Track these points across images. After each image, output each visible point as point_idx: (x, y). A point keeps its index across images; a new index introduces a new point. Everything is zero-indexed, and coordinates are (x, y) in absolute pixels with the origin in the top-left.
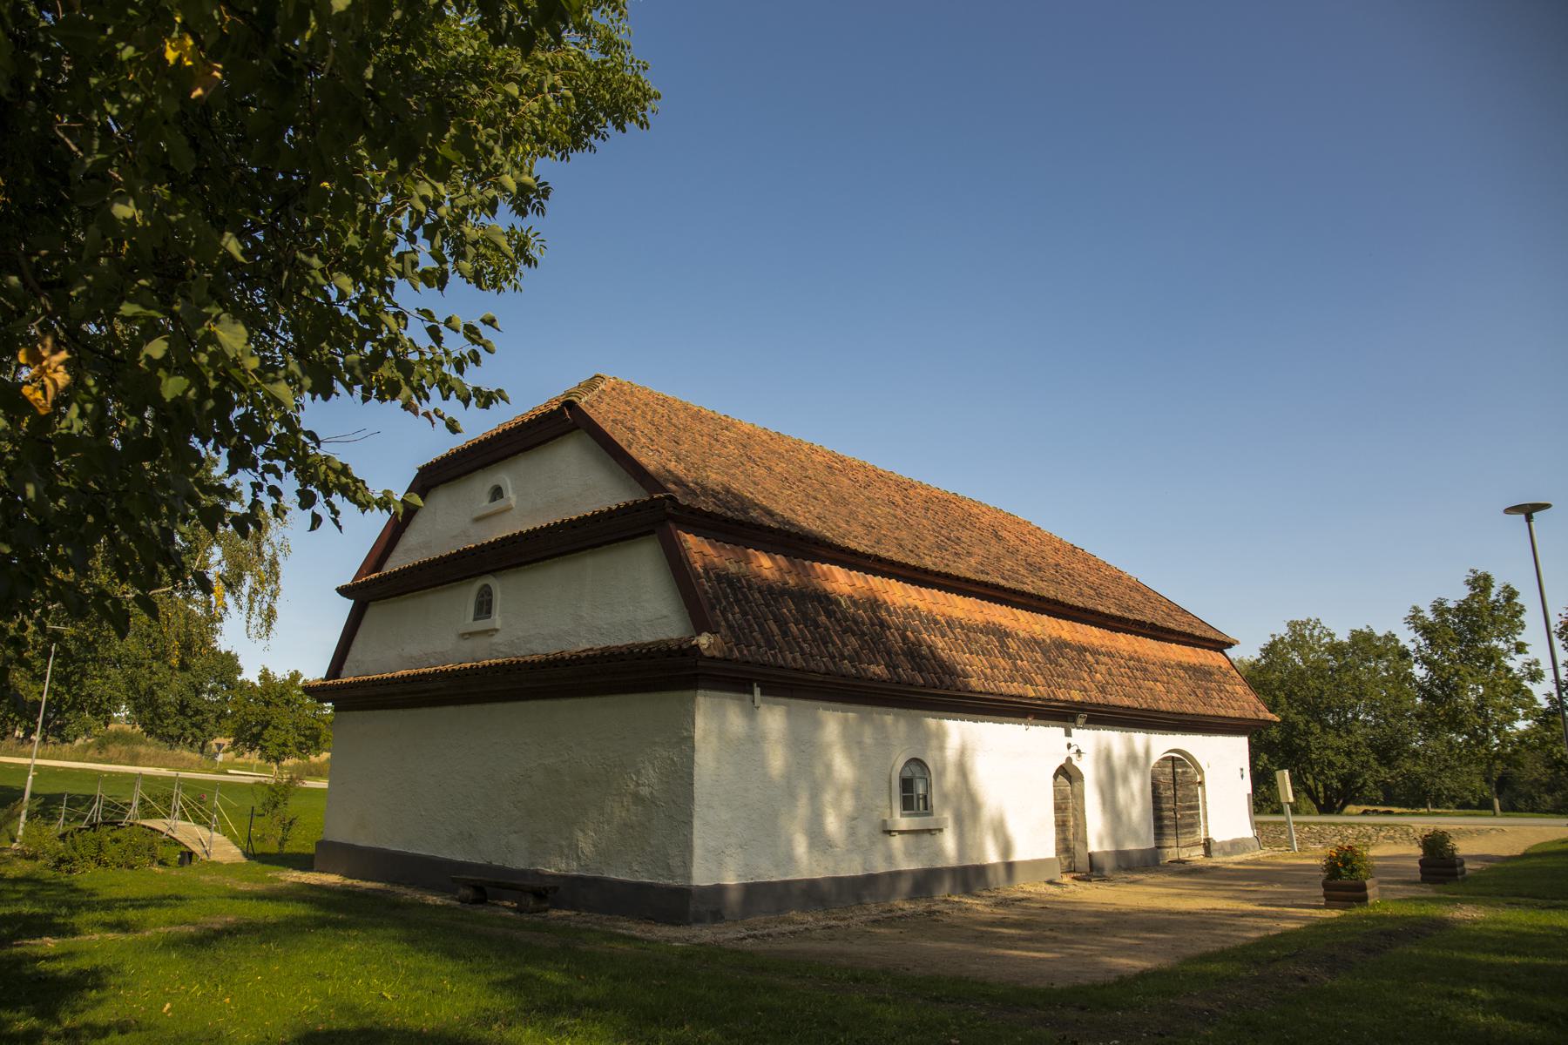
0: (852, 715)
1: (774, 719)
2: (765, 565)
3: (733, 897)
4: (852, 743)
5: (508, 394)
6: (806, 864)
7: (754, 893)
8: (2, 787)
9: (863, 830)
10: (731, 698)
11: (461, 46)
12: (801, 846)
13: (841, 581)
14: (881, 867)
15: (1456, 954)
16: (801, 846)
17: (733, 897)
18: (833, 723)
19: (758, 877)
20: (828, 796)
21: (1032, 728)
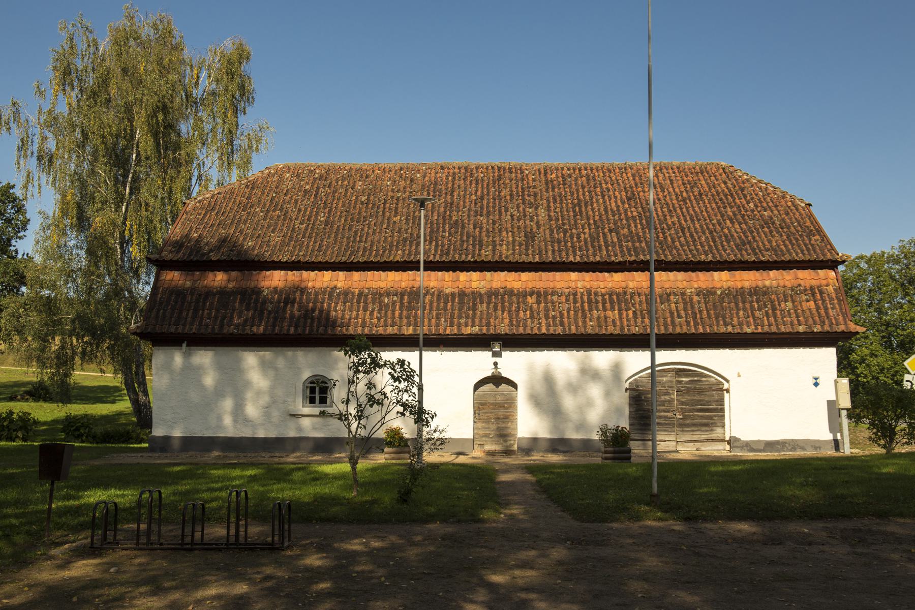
0: (267, 354)
1: (204, 358)
2: (219, 278)
3: (176, 445)
4: (264, 366)
5: (730, 382)
6: (228, 427)
7: (189, 442)
8: (6, 386)
9: (275, 414)
10: (175, 349)
11: (292, 217)
12: (228, 421)
13: (276, 279)
14: (292, 434)
15: (456, 320)
16: (228, 421)
17: (176, 445)
18: (251, 359)
19: (195, 433)
20: (249, 395)
21: (444, 353)
